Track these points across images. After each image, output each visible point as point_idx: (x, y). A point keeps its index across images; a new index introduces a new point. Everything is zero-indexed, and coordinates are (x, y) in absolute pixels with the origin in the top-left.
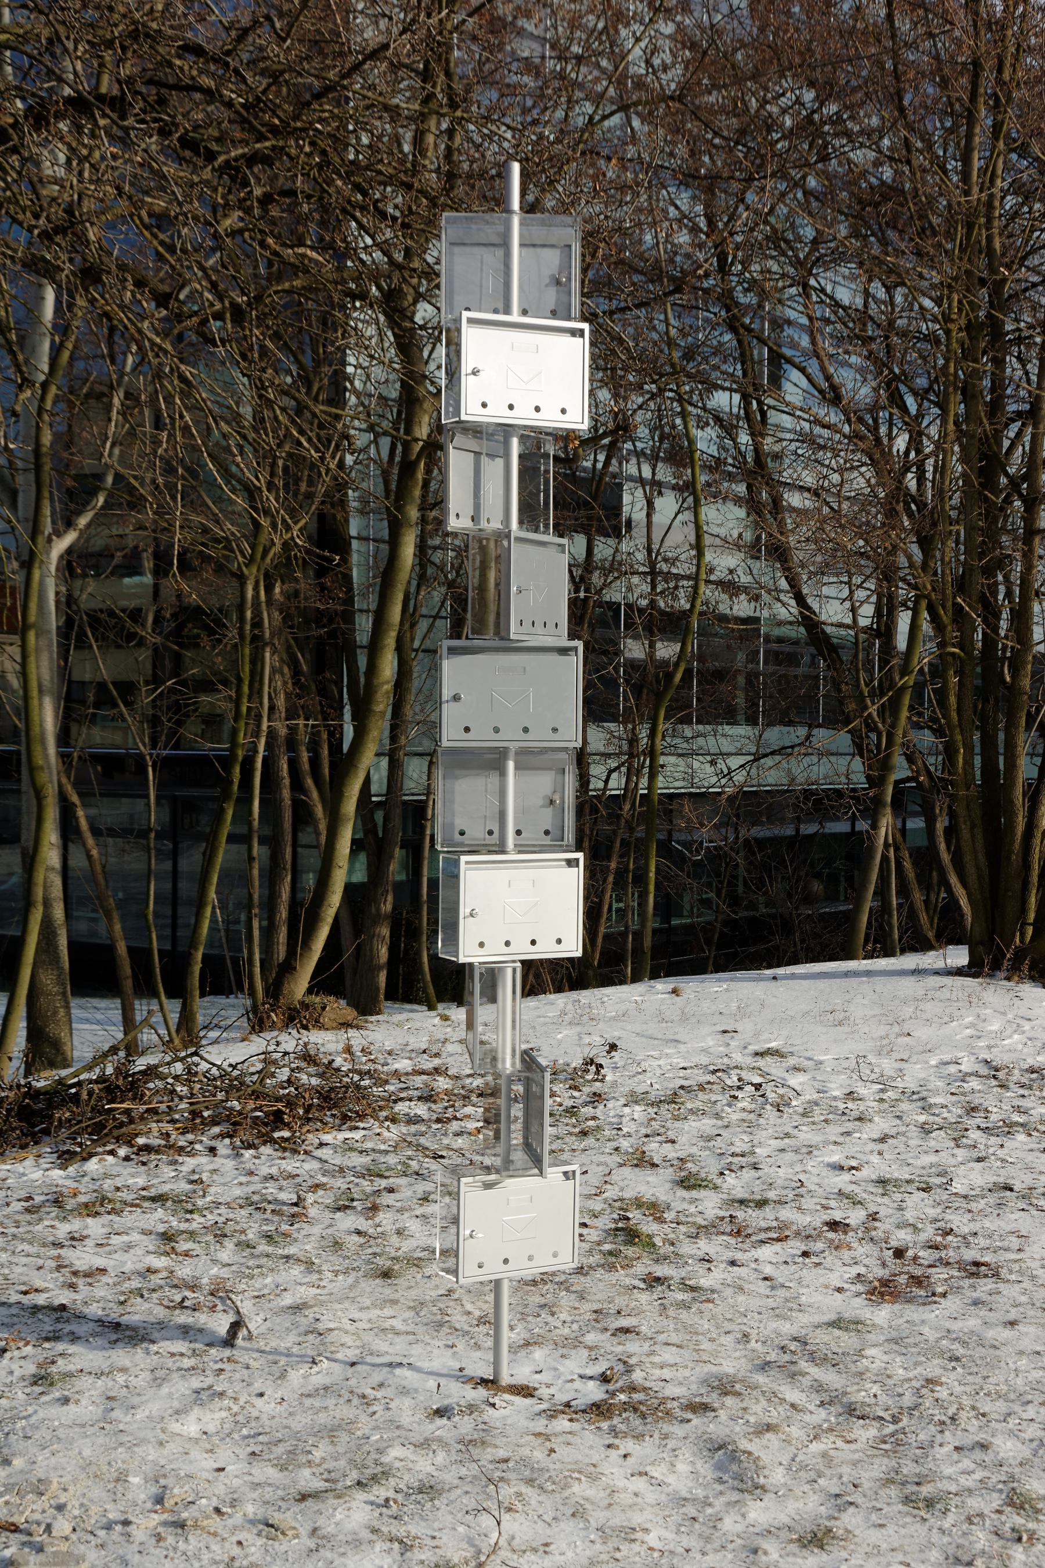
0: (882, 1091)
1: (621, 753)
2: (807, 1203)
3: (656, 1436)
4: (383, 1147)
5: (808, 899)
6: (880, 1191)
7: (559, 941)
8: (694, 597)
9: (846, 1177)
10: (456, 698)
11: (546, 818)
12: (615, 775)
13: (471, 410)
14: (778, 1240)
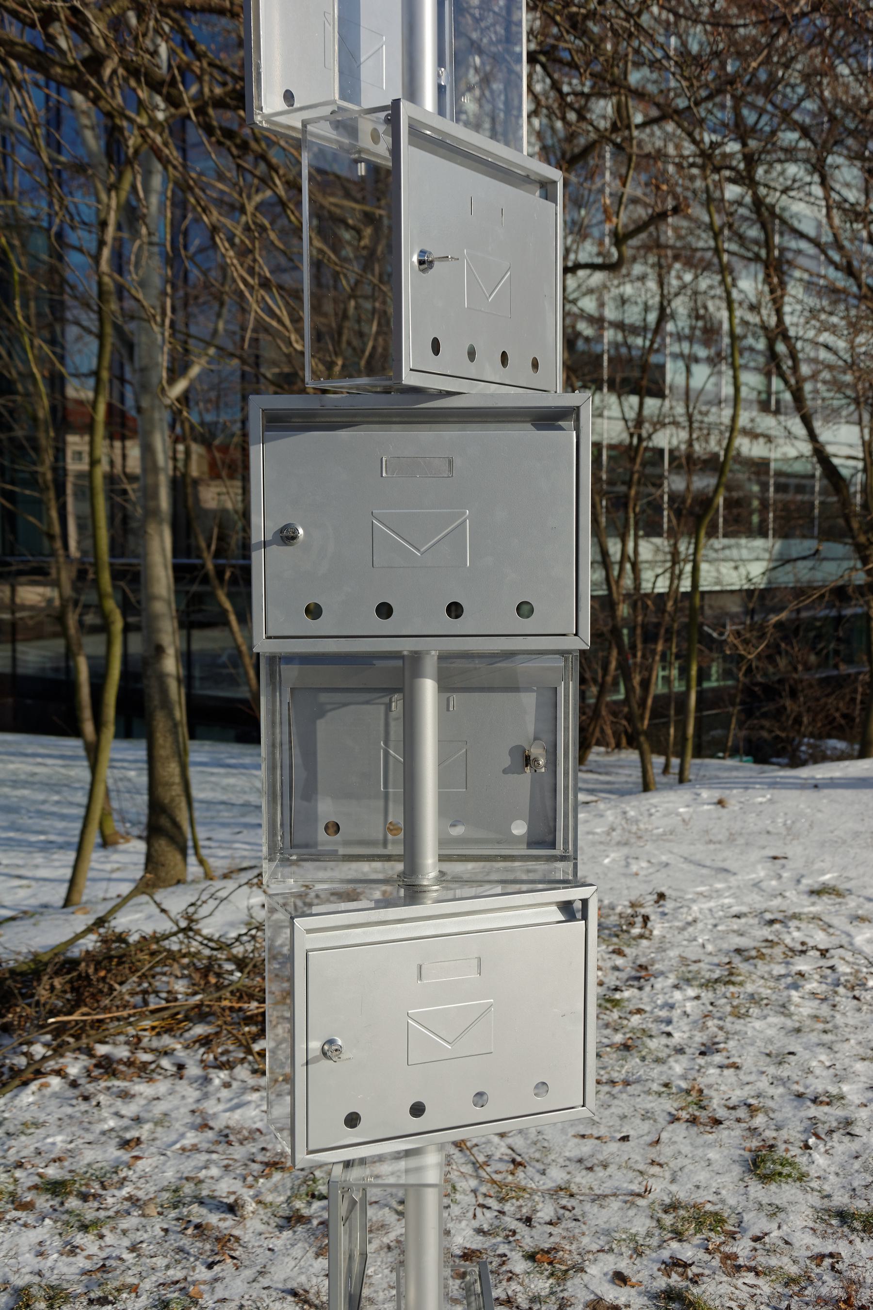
1: (665, 561)
12: (660, 579)
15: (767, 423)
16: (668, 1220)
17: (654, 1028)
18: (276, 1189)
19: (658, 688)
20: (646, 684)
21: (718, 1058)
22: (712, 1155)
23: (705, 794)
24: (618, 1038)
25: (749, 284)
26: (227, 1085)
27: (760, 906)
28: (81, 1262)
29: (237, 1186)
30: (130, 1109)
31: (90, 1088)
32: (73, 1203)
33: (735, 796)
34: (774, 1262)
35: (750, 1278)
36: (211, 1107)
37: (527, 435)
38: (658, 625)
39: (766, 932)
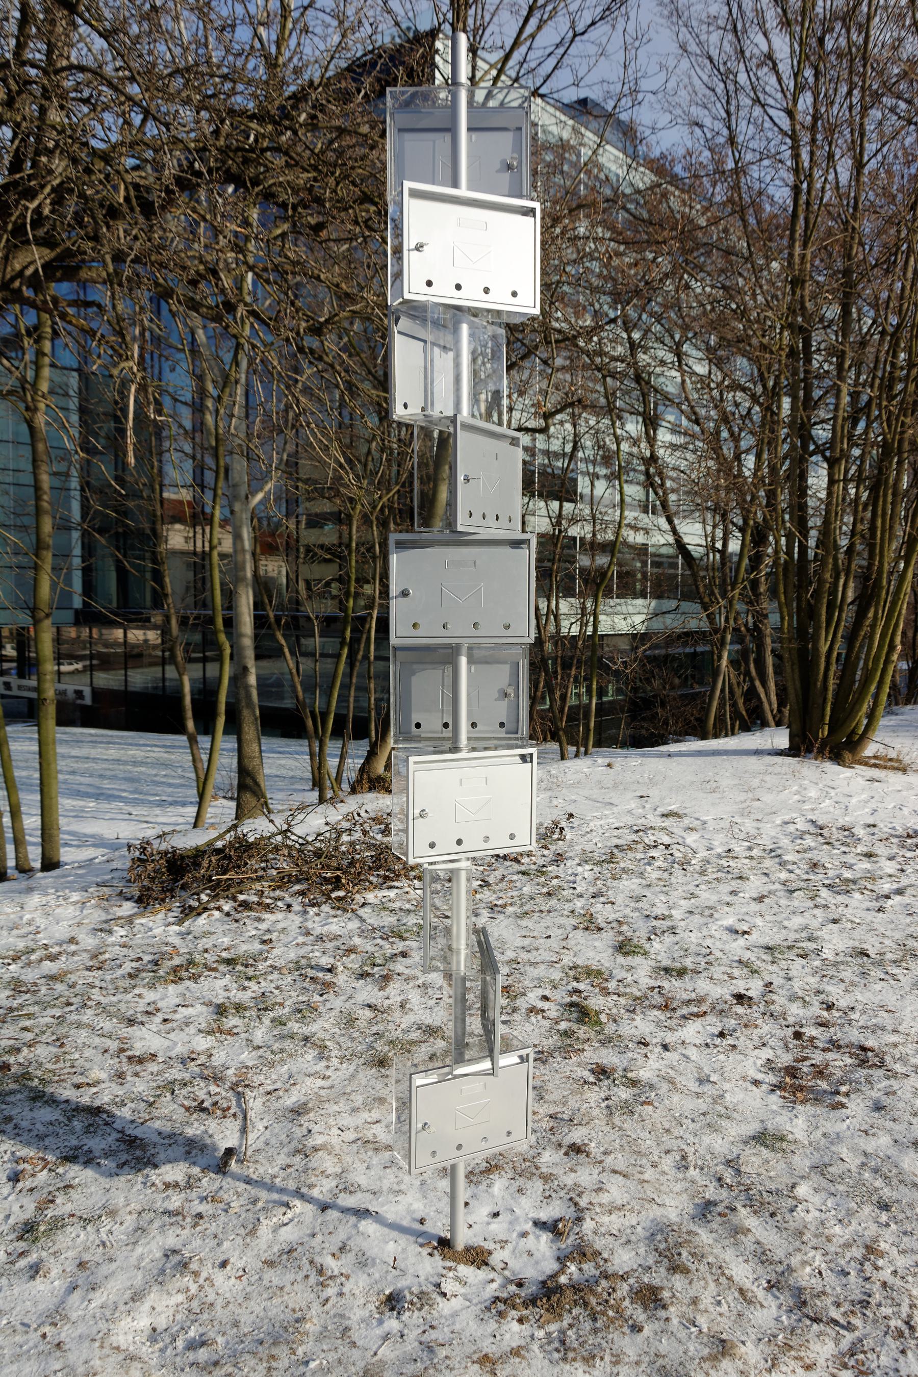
0: (750, 848)
2: (717, 972)
3: (607, 1358)
4: (408, 906)
5: (673, 688)
6: (769, 958)
7: (512, 837)
8: (617, 534)
9: (741, 941)
10: (405, 594)
11: (501, 711)
13: (414, 288)
14: (698, 1015)
15: (646, 520)
16: (572, 973)
17: (566, 886)
18: (354, 962)
19: (572, 701)
20: (563, 698)
21: (602, 899)
22: (597, 944)
23: (600, 761)
24: (545, 890)
25: (633, 427)
26: (318, 915)
27: (631, 823)
28: (249, 994)
29: (331, 961)
30: (264, 926)
31: (238, 916)
32: (239, 968)
33: (618, 762)
34: (628, 990)
35: (615, 997)
36: (309, 925)
37: (508, 551)
38: (572, 658)
39: (634, 837)
